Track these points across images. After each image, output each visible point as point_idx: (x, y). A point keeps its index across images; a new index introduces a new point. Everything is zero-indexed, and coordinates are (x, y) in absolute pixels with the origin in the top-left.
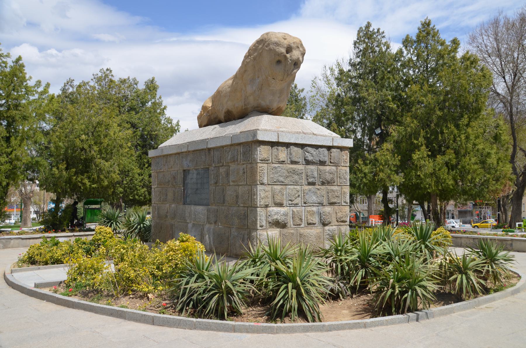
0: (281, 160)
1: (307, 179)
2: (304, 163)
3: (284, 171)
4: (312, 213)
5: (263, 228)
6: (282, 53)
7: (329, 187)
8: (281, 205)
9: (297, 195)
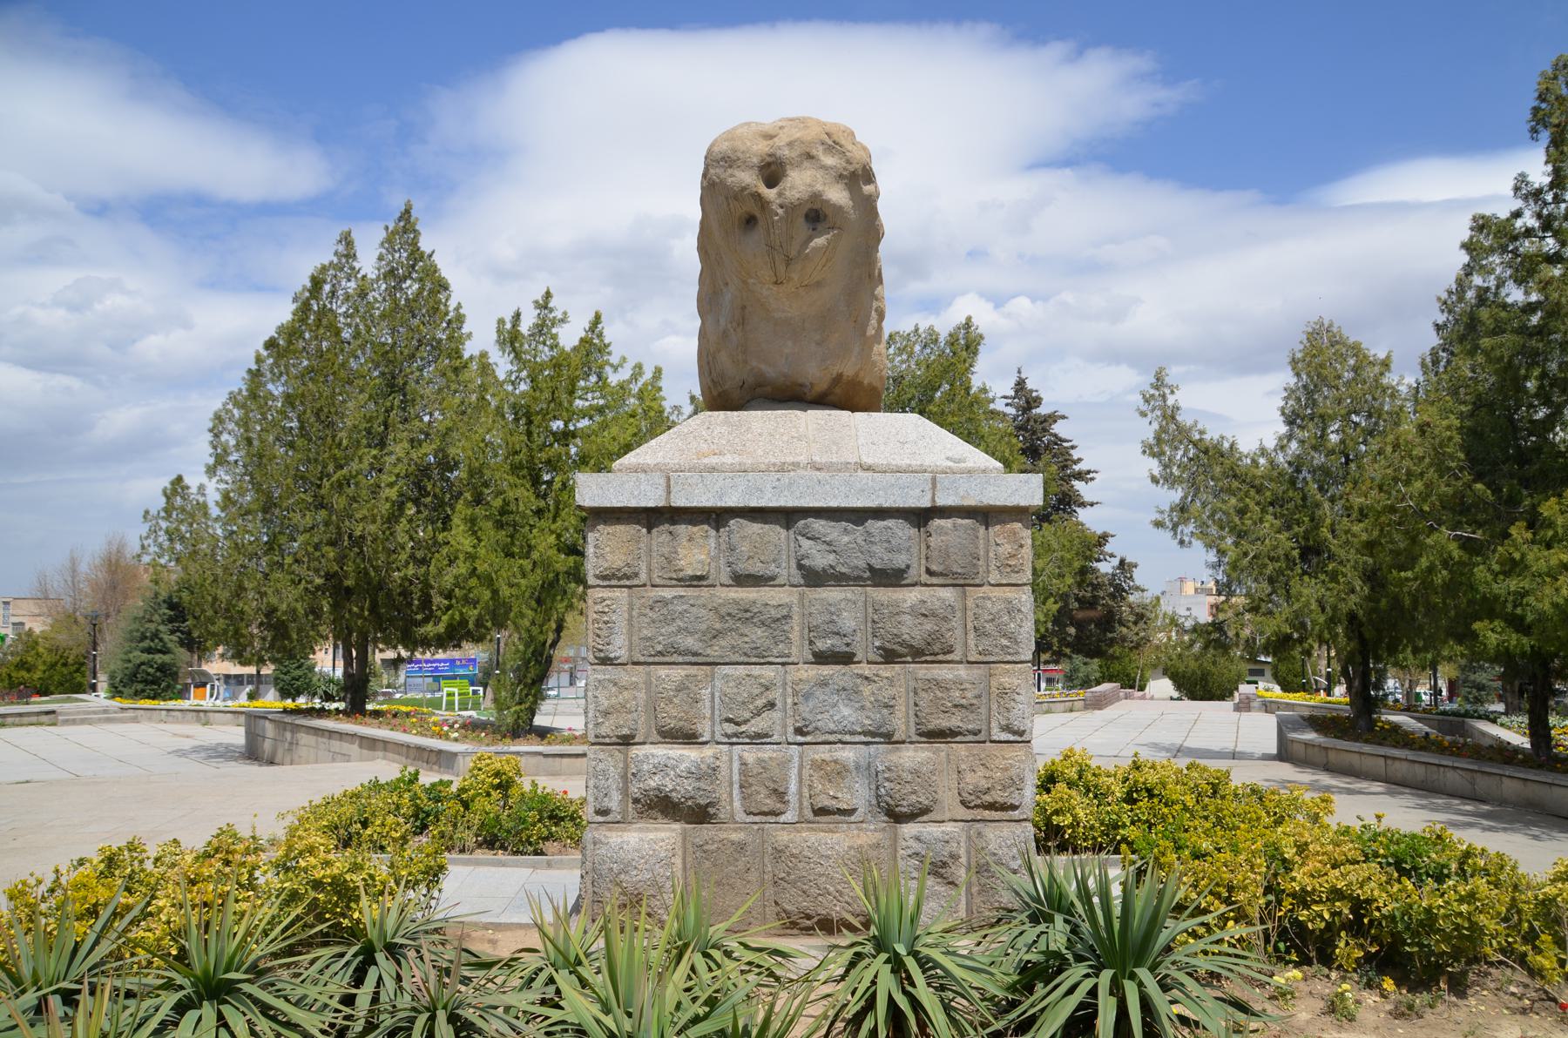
0: (690, 572)
1: (811, 643)
2: (798, 579)
4: (839, 772)
5: (609, 818)
6: (744, 189)
7: (922, 671)
9: (760, 702)
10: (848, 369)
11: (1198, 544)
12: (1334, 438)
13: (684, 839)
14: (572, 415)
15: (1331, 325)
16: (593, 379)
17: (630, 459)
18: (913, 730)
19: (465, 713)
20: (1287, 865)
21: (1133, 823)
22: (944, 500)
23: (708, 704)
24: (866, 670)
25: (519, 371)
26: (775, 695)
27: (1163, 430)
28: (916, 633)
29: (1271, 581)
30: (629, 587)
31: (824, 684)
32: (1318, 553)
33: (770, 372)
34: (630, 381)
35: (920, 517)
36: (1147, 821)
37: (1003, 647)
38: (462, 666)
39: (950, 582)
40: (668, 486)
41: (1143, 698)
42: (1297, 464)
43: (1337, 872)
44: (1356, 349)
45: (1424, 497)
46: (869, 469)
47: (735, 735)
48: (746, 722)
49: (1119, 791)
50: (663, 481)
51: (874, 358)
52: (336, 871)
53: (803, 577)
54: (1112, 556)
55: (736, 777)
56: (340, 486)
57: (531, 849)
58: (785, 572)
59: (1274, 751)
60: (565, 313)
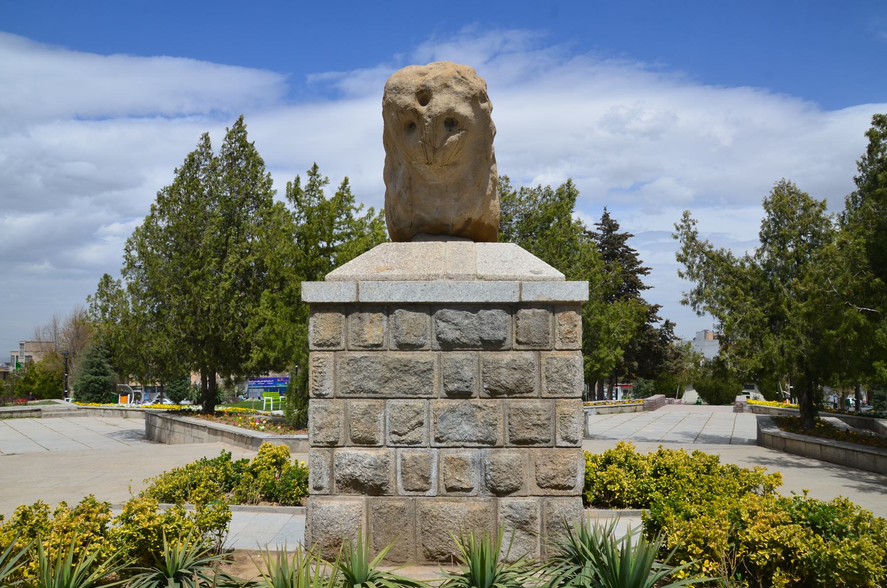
0: (371, 342)
1: (445, 385)
2: (437, 347)
3: (379, 366)
4: (461, 465)
5: (322, 492)
6: (407, 106)
7: (513, 403)
8: (370, 443)
9: (413, 422)
10: (475, 215)
11: (708, 313)
12: (790, 250)
13: (367, 505)
14: (331, 239)
15: (789, 183)
16: (344, 217)
17: (336, 272)
18: (508, 439)
19: (275, 412)
20: (744, 525)
21: (657, 489)
22: (526, 298)
23: (382, 423)
24: (479, 402)
25: (300, 212)
26: (423, 417)
27: (687, 247)
28: (509, 380)
29: (752, 336)
30: (335, 351)
31: (453, 411)
32: (780, 319)
33: (427, 217)
34: (365, 218)
35: (512, 308)
36: (666, 488)
37: (564, 389)
38: (281, 382)
39: (531, 348)
40: (358, 290)
41: (680, 403)
42: (768, 266)
43: (774, 530)
44: (805, 198)
45: (842, 286)
46: (481, 278)
47: (399, 442)
48: (405, 434)
49: (649, 470)
50: (354, 287)
51: (491, 208)
52: (156, 523)
53: (440, 345)
54: (660, 319)
55: (399, 468)
56: (195, 280)
57: (292, 502)
58: (429, 342)
59: (755, 438)
60: (327, 178)
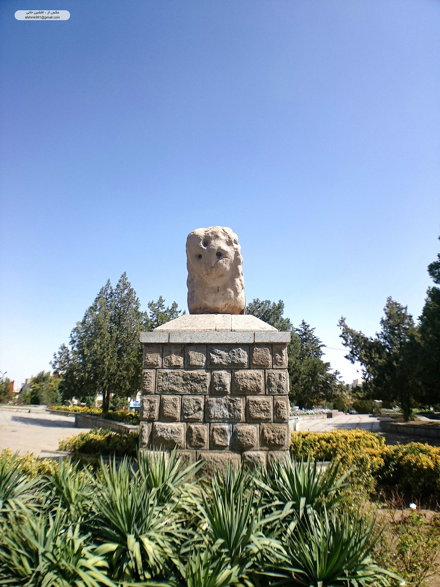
17: (159, 328)
